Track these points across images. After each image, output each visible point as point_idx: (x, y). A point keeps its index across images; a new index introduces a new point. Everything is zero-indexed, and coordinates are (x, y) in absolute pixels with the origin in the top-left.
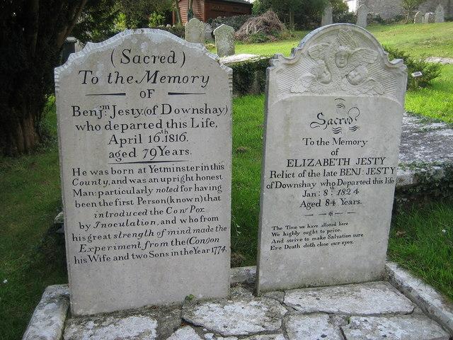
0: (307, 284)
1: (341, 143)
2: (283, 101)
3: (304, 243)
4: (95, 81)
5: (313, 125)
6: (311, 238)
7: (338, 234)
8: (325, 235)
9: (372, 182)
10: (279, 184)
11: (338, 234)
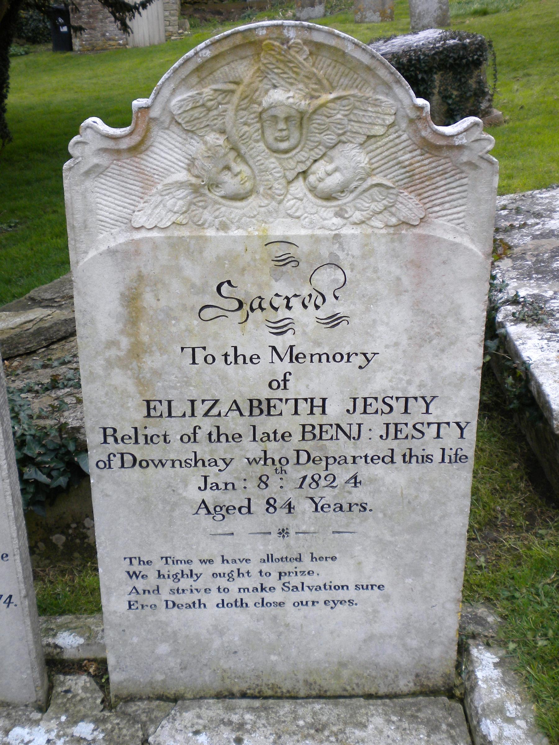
0: (236, 689)
1: (295, 358)
2: (112, 252)
3: (215, 597)
4: (210, 359)
5: (208, 313)
6: (233, 587)
7: (308, 580)
8: (272, 581)
9: (398, 458)
10: (128, 459)
11: (308, 580)
